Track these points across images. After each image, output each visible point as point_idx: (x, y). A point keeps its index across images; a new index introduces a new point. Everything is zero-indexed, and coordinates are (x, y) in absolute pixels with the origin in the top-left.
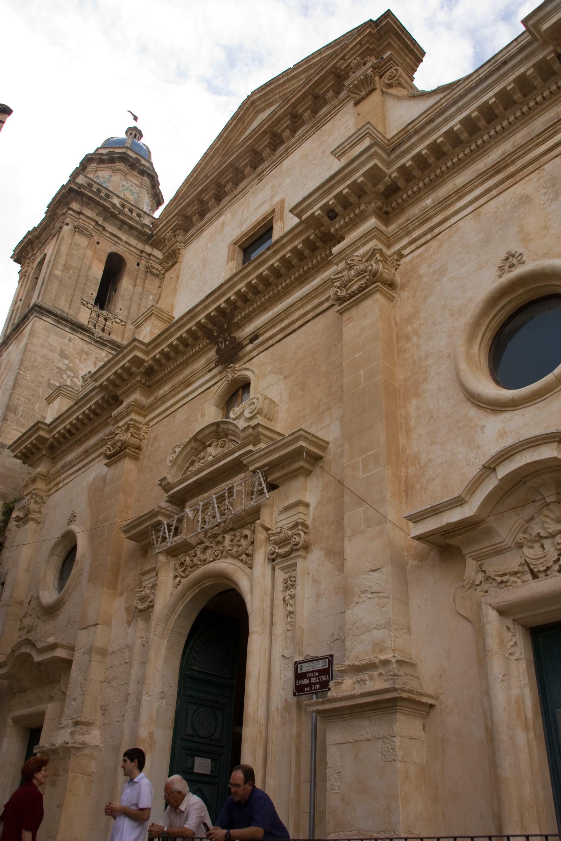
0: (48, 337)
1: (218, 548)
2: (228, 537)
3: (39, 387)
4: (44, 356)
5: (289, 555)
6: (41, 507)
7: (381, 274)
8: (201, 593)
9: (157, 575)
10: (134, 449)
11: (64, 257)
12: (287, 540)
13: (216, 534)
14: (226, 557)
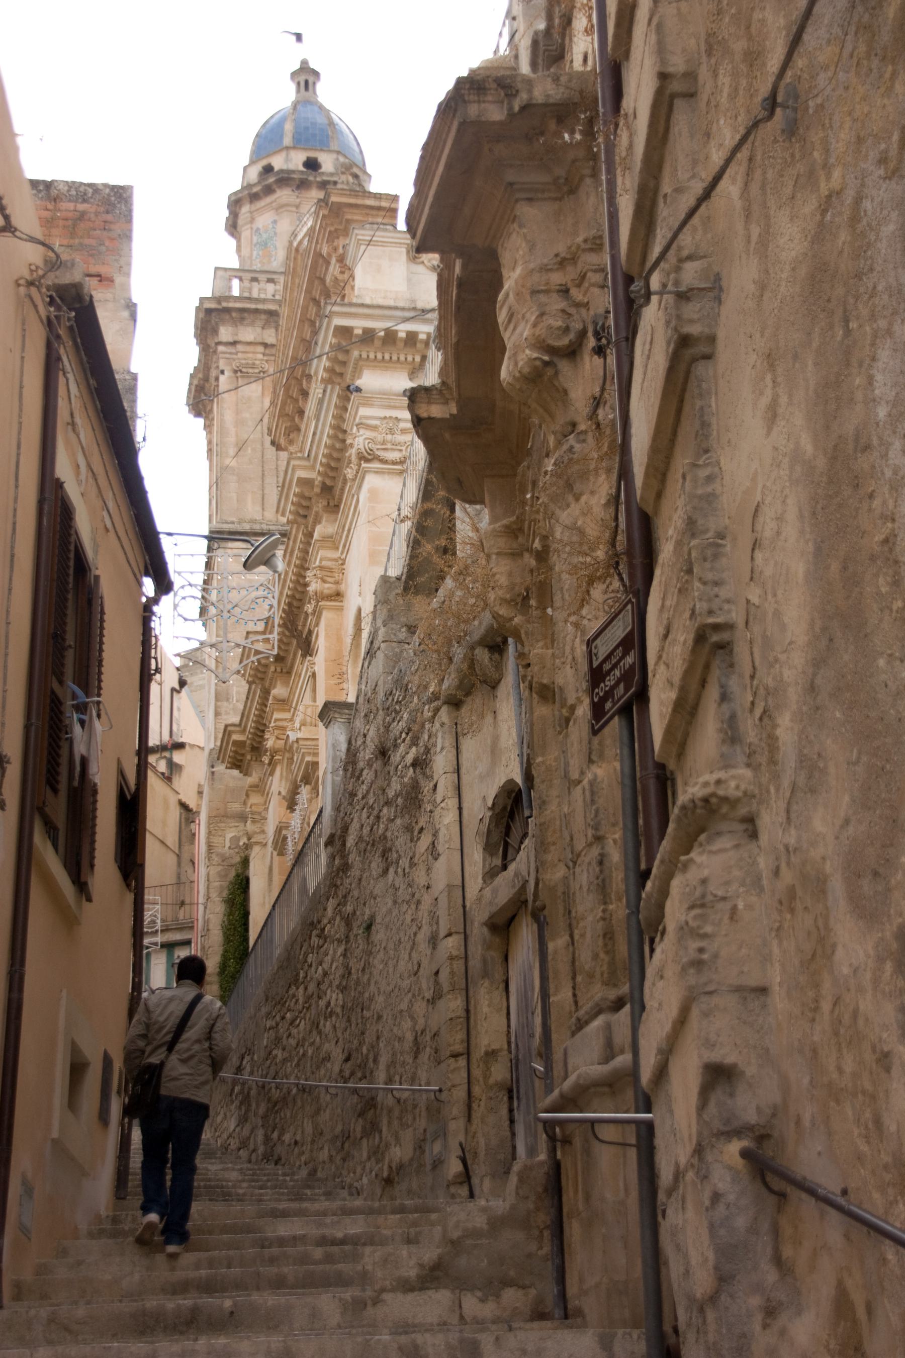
7: (322, 593)
11: (233, 430)
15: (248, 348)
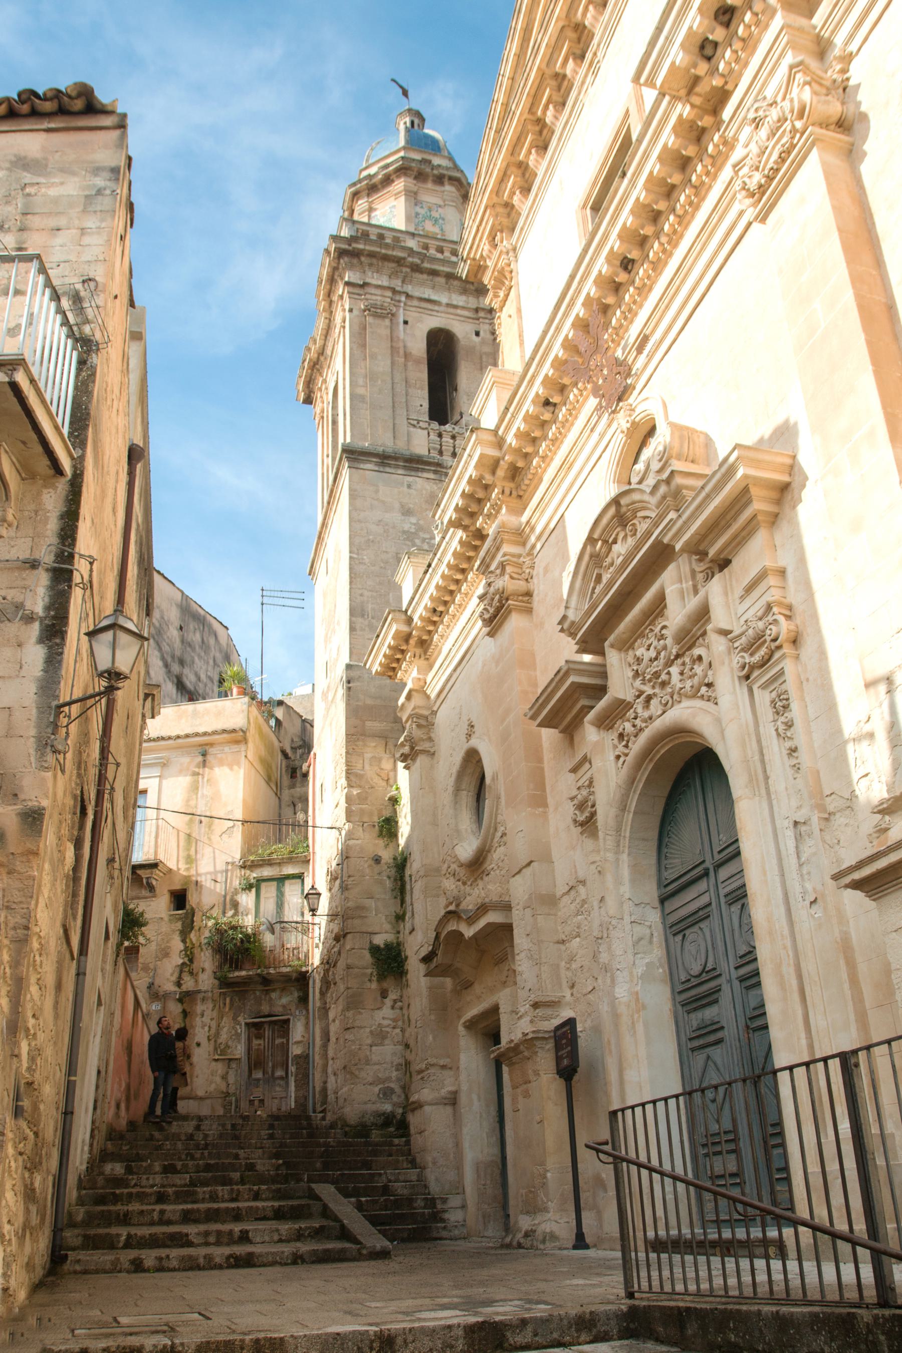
0: (377, 491)
1: (664, 692)
2: (675, 670)
3: (385, 568)
4: (380, 521)
5: (769, 660)
6: (429, 730)
8: (656, 770)
9: (590, 763)
10: (520, 598)
12: (760, 639)
13: (656, 672)
14: (680, 702)
15: (378, 292)
